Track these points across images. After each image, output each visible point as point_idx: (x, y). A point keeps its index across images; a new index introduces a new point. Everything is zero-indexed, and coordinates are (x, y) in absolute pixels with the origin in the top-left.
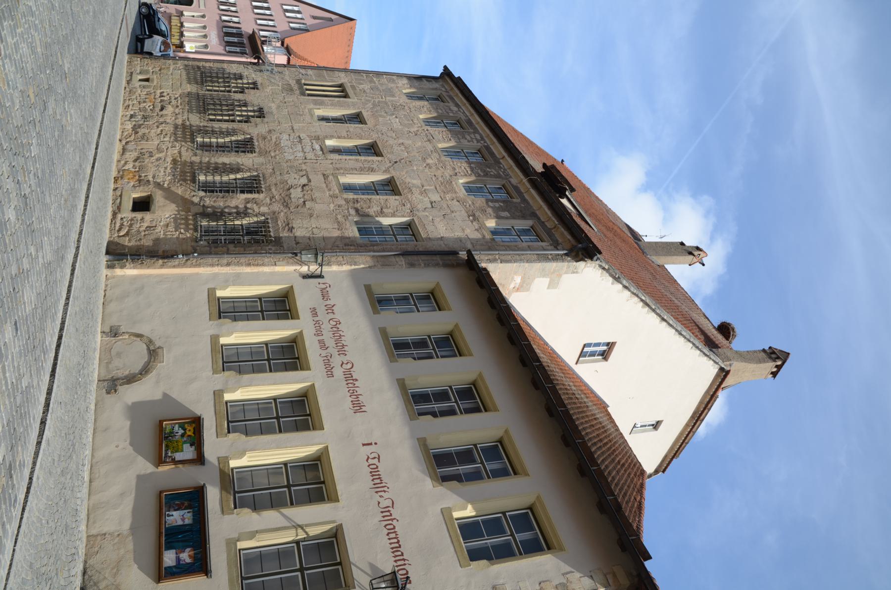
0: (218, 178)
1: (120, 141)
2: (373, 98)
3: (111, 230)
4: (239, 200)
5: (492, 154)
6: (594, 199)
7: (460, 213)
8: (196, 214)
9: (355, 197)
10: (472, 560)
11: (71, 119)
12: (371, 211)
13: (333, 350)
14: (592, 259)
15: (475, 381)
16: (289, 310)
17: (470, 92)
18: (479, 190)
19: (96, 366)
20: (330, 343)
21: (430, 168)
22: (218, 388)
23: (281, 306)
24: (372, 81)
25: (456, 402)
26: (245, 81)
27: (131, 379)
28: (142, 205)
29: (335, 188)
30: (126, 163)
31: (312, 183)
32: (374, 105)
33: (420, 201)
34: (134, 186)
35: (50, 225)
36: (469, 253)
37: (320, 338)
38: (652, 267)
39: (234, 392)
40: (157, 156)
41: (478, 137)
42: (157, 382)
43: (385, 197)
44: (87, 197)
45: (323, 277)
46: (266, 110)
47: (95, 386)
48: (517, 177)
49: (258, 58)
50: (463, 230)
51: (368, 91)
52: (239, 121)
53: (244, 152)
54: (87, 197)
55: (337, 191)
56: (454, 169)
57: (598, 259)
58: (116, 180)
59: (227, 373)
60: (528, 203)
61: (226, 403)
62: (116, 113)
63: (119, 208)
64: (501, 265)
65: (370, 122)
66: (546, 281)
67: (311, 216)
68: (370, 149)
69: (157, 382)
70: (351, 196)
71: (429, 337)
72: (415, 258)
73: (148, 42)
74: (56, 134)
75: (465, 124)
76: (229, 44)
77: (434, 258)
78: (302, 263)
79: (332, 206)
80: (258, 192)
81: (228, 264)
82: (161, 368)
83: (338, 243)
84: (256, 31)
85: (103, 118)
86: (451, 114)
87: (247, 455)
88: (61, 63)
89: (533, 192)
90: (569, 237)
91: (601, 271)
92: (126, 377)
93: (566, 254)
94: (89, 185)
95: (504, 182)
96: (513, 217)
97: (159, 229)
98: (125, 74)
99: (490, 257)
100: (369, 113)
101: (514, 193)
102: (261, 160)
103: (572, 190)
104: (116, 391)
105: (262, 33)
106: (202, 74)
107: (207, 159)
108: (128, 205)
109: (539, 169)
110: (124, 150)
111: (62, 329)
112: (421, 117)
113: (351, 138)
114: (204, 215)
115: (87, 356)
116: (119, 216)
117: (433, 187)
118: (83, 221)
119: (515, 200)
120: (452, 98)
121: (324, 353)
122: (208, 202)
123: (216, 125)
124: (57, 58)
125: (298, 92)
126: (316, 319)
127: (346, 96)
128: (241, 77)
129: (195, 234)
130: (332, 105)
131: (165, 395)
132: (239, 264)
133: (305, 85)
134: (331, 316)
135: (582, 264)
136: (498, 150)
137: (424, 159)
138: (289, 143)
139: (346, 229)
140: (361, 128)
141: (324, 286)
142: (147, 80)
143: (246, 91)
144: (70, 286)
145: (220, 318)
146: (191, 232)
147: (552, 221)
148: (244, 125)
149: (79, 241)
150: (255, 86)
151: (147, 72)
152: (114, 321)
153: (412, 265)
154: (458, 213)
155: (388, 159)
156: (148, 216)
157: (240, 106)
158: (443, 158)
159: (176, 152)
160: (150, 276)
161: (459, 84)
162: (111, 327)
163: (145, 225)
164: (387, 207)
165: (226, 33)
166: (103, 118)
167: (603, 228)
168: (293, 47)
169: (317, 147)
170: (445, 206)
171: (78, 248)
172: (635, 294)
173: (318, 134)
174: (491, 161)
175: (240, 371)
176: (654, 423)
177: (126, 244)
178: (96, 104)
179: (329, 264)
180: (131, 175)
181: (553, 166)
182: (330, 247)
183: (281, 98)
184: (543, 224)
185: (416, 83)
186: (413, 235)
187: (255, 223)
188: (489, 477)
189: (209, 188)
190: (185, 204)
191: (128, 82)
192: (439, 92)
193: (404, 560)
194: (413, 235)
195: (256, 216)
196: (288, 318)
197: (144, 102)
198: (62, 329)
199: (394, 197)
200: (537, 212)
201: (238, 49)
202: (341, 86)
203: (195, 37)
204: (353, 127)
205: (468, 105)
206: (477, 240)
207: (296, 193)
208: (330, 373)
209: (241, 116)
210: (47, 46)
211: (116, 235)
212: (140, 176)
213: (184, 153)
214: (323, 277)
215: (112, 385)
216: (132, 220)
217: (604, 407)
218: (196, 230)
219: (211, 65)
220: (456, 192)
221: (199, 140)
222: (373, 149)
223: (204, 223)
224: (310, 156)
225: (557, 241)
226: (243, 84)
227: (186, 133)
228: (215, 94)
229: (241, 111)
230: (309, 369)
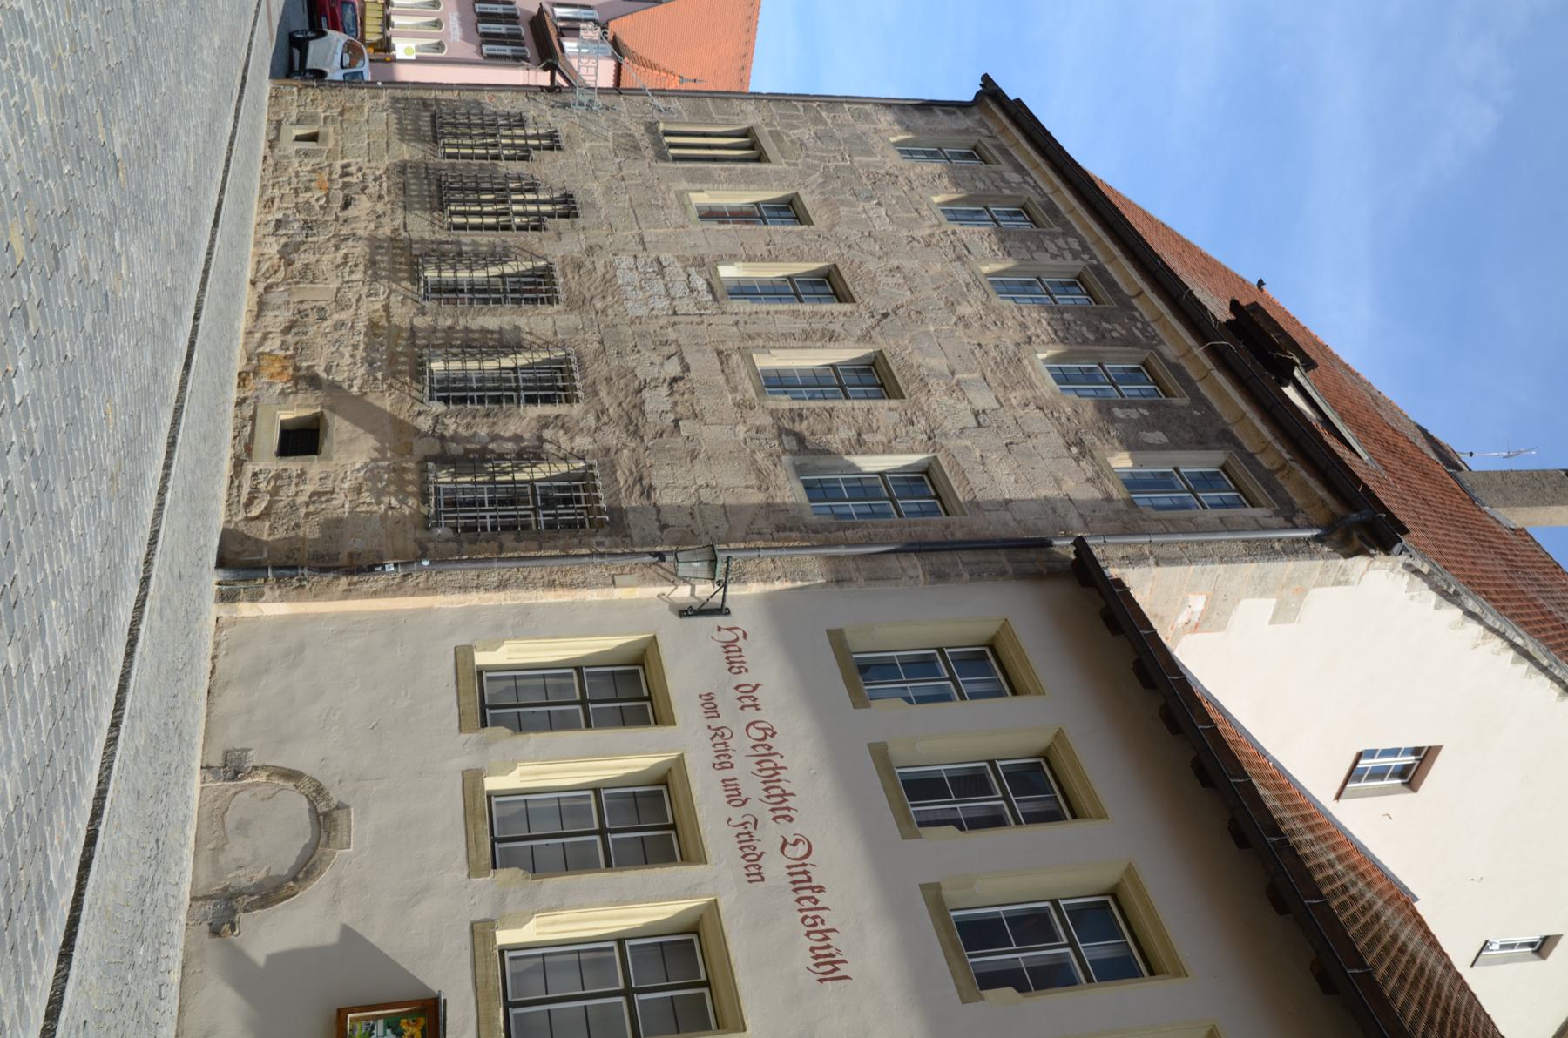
0: (473, 365)
1: (253, 283)
2: (822, 159)
3: (229, 505)
4: (524, 419)
5: (1111, 285)
6: (1340, 371)
7: (1048, 440)
8: (427, 459)
9: (796, 405)
10: (983, 988)
11: (130, 268)
12: (836, 441)
13: (759, 808)
14: (1387, 549)
15: (1117, 886)
16: (649, 698)
17: (1047, 134)
18: (1089, 377)
19: (188, 865)
20: (752, 787)
21: (967, 326)
22: (480, 914)
23: (624, 690)
24: (817, 120)
25: (1006, 798)
26: (531, 132)
27: (270, 894)
28: (301, 440)
29: (748, 384)
30: (265, 338)
31: (692, 375)
32: (827, 177)
33: (948, 410)
34: (282, 393)
35: (67, 562)
36: (1080, 544)
37: (727, 774)
38: (1499, 535)
39: (521, 925)
40: (336, 317)
41: (1076, 246)
42: (335, 901)
43: (866, 404)
44: (172, 444)
45: (728, 612)
46: (579, 199)
47: (183, 918)
48: (1177, 342)
49: (552, 68)
50: (1058, 482)
51: (810, 144)
52: (520, 228)
53: (534, 301)
54: (172, 444)
55: (752, 393)
56: (1024, 327)
57: (1404, 550)
58: (243, 378)
59: (503, 874)
60: (1209, 407)
61: (502, 952)
62: (243, 220)
63: (249, 449)
64: (1156, 571)
65: (820, 218)
66: (1270, 603)
67: (694, 456)
68: (821, 283)
69: (335, 901)
70: (784, 403)
71: (992, 763)
72: (946, 558)
73: (314, 47)
74: (88, 322)
75: (1041, 215)
76: (488, 38)
77: (993, 556)
78: (675, 578)
79: (741, 429)
80: (568, 400)
81: (502, 586)
82: (343, 862)
83: (761, 523)
84: (547, 7)
85: (213, 240)
86: (1007, 192)
87: (519, 769)
88: (102, 138)
89: (1220, 378)
90: (1322, 493)
91: (1407, 576)
92: (259, 885)
93: (1317, 539)
94: (178, 411)
95: (1146, 354)
96: (1176, 445)
97: (339, 499)
98: (264, 127)
99: (1129, 550)
100: (816, 196)
101: (1171, 382)
102: (573, 319)
103: (1309, 364)
104: (233, 928)
105: (559, 12)
106: (433, 116)
107: (449, 322)
108: (269, 439)
109: (1223, 313)
110: (262, 306)
111: (96, 815)
112: (937, 199)
113: (776, 259)
114: (443, 460)
115: (164, 851)
116: (249, 468)
117: (977, 375)
118: (160, 506)
119: (1176, 401)
120: (1005, 152)
121: (738, 815)
122: (451, 426)
123: (466, 238)
124: (93, 129)
125: (651, 153)
126: (716, 723)
127: (761, 158)
128: (521, 123)
129: (424, 510)
130: (729, 180)
131: (347, 933)
132: (527, 584)
133: (667, 134)
134: (751, 715)
135: (1360, 562)
136: (1126, 275)
137: (951, 306)
138: (635, 277)
139: (777, 487)
140: (800, 235)
141: (730, 636)
142: (313, 138)
143: (534, 154)
144: (122, 689)
145: (484, 724)
146: (412, 502)
147: (1273, 453)
148: (531, 237)
149: (148, 562)
150: (553, 142)
151: (312, 119)
152: (232, 737)
153: (939, 576)
154: (1042, 439)
155: (867, 307)
156: (314, 467)
157: (520, 191)
158: (997, 301)
159: (378, 306)
160: (318, 618)
161: (1019, 114)
162: (226, 753)
163: (309, 488)
164: (871, 430)
165: (484, 35)
166: (213, 240)
167: (1377, 448)
168: (625, 39)
169: (700, 284)
170: (1009, 421)
171: (145, 581)
172: (1496, 631)
173: (701, 251)
174: (1110, 303)
175: (534, 868)
176: (1535, 937)
177: (265, 537)
178: (195, 211)
179: (740, 580)
180: (276, 367)
181: (1255, 307)
182: (740, 534)
183: (614, 168)
184: (1250, 459)
185: (919, 120)
186: (938, 497)
187: (545, 361)
188: (1089, 980)
189: (453, 392)
190: (398, 433)
191: (272, 144)
192: (974, 139)
193: (829, 947)
194: (938, 497)
195: (565, 459)
196: (646, 723)
197: (308, 189)
198: (96, 815)
199: (886, 403)
200: (1235, 430)
201: (508, 50)
202: (746, 133)
203: (417, 26)
204: (781, 231)
205: (1044, 167)
206: (1093, 505)
207: (657, 401)
208: (756, 875)
209: (513, 146)
210: (64, 105)
211: (241, 516)
212: (297, 369)
213: (396, 309)
214: (728, 612)
215: (223, 910)
216: (278, 477)
217: (1403, 900)
218: (424, 497)
219: (454, 95)
220: (1032, 386)
221: (431, 274)
222: (829, 285)
223: (444, 477)
224: (685, 305)
225: (1291, 502)
226: (526, 137)
227: (399, 258)
228: (462, 164)
229: (523, 202)
230: (702, 859)
